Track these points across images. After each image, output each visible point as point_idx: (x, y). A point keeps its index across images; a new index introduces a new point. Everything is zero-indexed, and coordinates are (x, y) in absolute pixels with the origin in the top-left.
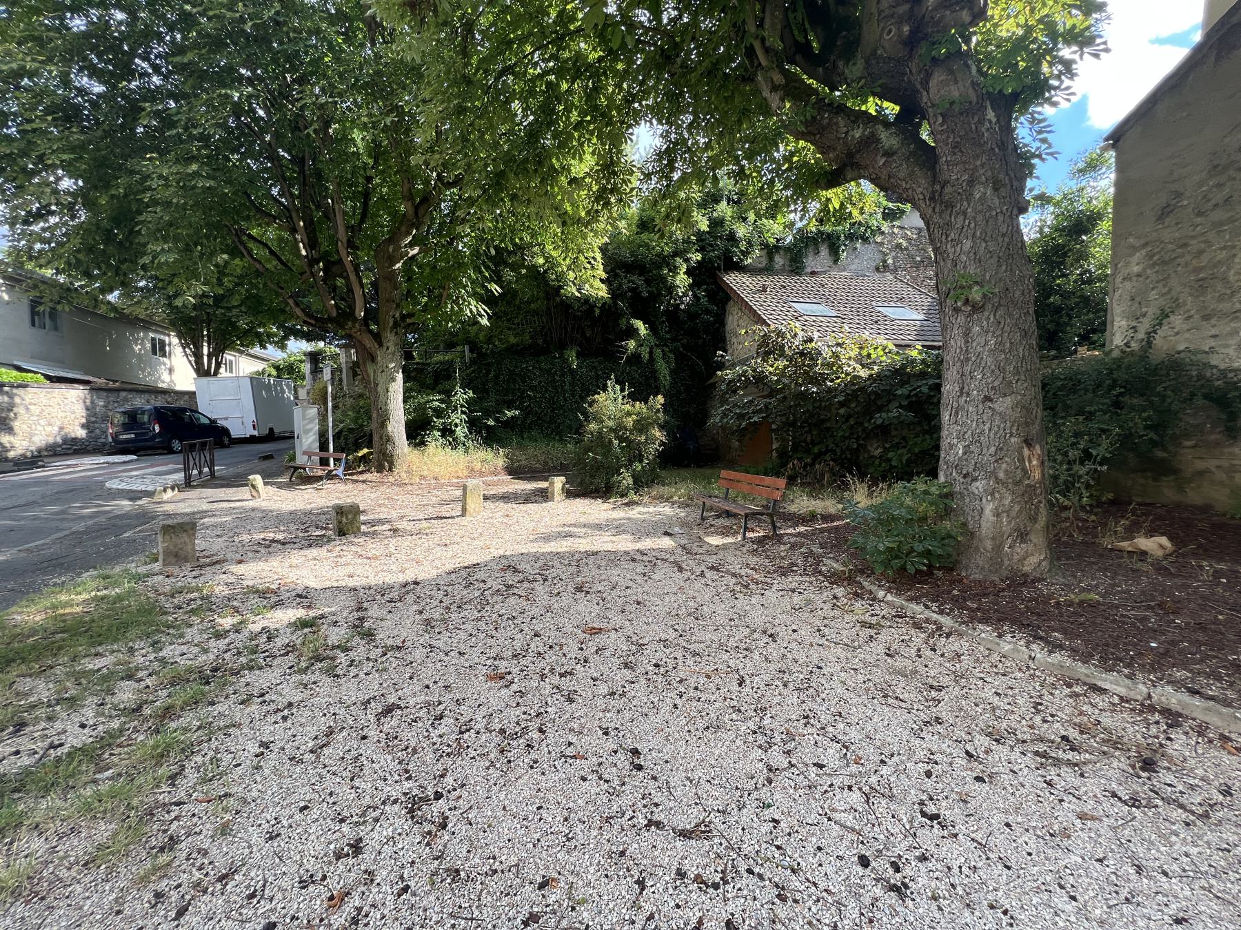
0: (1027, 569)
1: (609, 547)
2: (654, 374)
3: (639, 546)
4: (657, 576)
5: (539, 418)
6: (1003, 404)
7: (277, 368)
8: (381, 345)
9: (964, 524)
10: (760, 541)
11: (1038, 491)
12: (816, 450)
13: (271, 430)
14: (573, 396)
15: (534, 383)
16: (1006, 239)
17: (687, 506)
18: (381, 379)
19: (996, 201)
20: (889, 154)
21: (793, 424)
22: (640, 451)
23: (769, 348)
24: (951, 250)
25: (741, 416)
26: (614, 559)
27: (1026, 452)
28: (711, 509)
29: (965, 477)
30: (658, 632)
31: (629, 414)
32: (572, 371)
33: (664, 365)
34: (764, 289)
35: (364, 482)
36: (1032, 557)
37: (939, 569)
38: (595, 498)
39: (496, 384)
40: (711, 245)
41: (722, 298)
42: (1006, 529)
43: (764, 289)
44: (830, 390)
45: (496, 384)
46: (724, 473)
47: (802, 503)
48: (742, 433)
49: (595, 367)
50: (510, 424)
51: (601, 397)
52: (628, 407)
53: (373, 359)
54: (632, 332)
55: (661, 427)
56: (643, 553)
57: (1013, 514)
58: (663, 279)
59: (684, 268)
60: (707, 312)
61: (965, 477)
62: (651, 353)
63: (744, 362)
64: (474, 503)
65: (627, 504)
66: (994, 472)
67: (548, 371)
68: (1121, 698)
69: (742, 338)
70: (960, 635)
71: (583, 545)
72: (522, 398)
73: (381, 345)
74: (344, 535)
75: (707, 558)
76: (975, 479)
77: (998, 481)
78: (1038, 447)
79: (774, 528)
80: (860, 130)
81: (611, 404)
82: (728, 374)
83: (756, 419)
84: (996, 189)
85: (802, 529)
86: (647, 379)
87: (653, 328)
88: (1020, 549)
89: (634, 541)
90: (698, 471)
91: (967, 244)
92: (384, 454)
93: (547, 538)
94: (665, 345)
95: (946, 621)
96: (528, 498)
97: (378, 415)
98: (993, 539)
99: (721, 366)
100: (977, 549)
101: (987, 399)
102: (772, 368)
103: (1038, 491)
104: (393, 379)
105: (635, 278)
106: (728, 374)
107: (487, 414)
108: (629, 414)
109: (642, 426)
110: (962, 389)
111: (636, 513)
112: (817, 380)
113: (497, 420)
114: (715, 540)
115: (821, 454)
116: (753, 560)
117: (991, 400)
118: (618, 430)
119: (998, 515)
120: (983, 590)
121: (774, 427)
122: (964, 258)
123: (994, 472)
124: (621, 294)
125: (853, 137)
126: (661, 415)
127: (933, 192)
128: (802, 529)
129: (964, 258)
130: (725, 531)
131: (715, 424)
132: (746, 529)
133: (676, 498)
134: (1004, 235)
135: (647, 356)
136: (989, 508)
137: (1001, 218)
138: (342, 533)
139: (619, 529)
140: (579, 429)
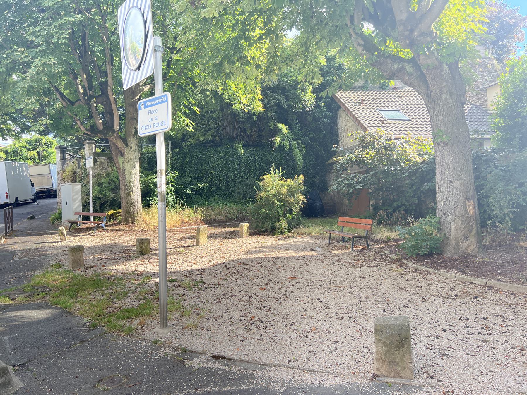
0: (469, 252)
1: (282, 255)
2: (292, 158)
3: (299, 255)
4: (312, 264)
5: (218, 188)
6: (457, 184)
7: (6, 152)
8: (127, 145)
9: (445, 234)
10: (361, 251)
11: (472, 220)
12: (395, 204)
13: (17, 198)
14: (240, 173)
15: (215, 165)
16: (456, 116)
17: (320, 238)
18: (127, 166)
19: (451, 101)
20: (410, 75)
21: (381, 189)
22: (290, 207)
23: (365, 144)
24: (435, 119)
25: (349, 185)
26: (290, 259)
27: (467, 203)
28: (334, 239)
29: (444, 215)
30: (319, 278)
31: (283, 186)
32: (239, 158)
33: (299, 152)
34: (362, 102)
35: (119, 230)
36: (471, 246)
37: (435, 254)
38: (266, 235)
39: (190, 166)
40: (328, 73)
41: (334, 106)
42: (460, 235)
43: (362, 102)
44: (402, 169)
45: (190, 166)
46: (340, 219)
47: (384, 233)
48: (350, 196)
49: (253, 154)
50: (199, 193)
51: (267, 177)
52: (282, 182)
53: (122, 154)
54: (277, 131)
55: (303, 193)
56: (303, 257)
57: (462, 229)
58: (298, 97)
59: (311, 88)
60: (326, 117)
61: (444, 215)
62: (290, 145)
63: (350, 150)
64: (203, 239)
65: (285, 238)
66: (454, 212)
67: (223, 158)
68: (479, 285)
69: (348, 137)
70: (435, 273)
71: (271, 255)
72: (207, 175)
73: (127, 145)
74: (143, 254)
75: (335, 258)
76: (448, 216)
77: (456, 216)
78: (472, 201)
79: (368, 246)
80: (397, 65)
81: (273, 182)
82: (341, 159)
83: (358, 187)
84: (451, 96)
85: (382, 245)
86: (287, 161)
87: (290, 129)
88: (466, 243)
89: (296, 253)
90: (325, 220)
91: (441, 117)
92: (129, 213)
93: (251, 252)
94: (299, 139)
95: (431, 270)
96: (226, 236)
97: (126, 189)
98: (455, 240)
99: (334, 154)
100: (450, 244)
101: (451, 182)
102: (369, 154)
103: (472, 220)
104: (134, 167)
105: (278, 96)
106: (341, 159)
107: (186, 186)
108: (283, 186)
109: (291, 193)
110: (442, 177)
111: (291, 241)
112: (393, 163)
113: (192, 190)
114: (337, 252)
115: (399, 207)
116: (357, 258)
117: (452, 182)
118: (278, 196)
119: (456, 230)
120: (451, 260)
121: (370, 191)
122: (439, 123)
123: (454, 212)
124: (270, 107)
125: (394, 68)
126: (302, 186)
127: (428, 94)
128: (382, 245)
129: (439, 123)
130: (343, 248)
131: (333, 190)
132: (353, 246)
133: (313, 234)
134: (454, 114)
135: (288, 146)
136: (453, 227)
137: (453, 107)
138: (142, 254)
139: (286, 248)
140: (253, 197)
